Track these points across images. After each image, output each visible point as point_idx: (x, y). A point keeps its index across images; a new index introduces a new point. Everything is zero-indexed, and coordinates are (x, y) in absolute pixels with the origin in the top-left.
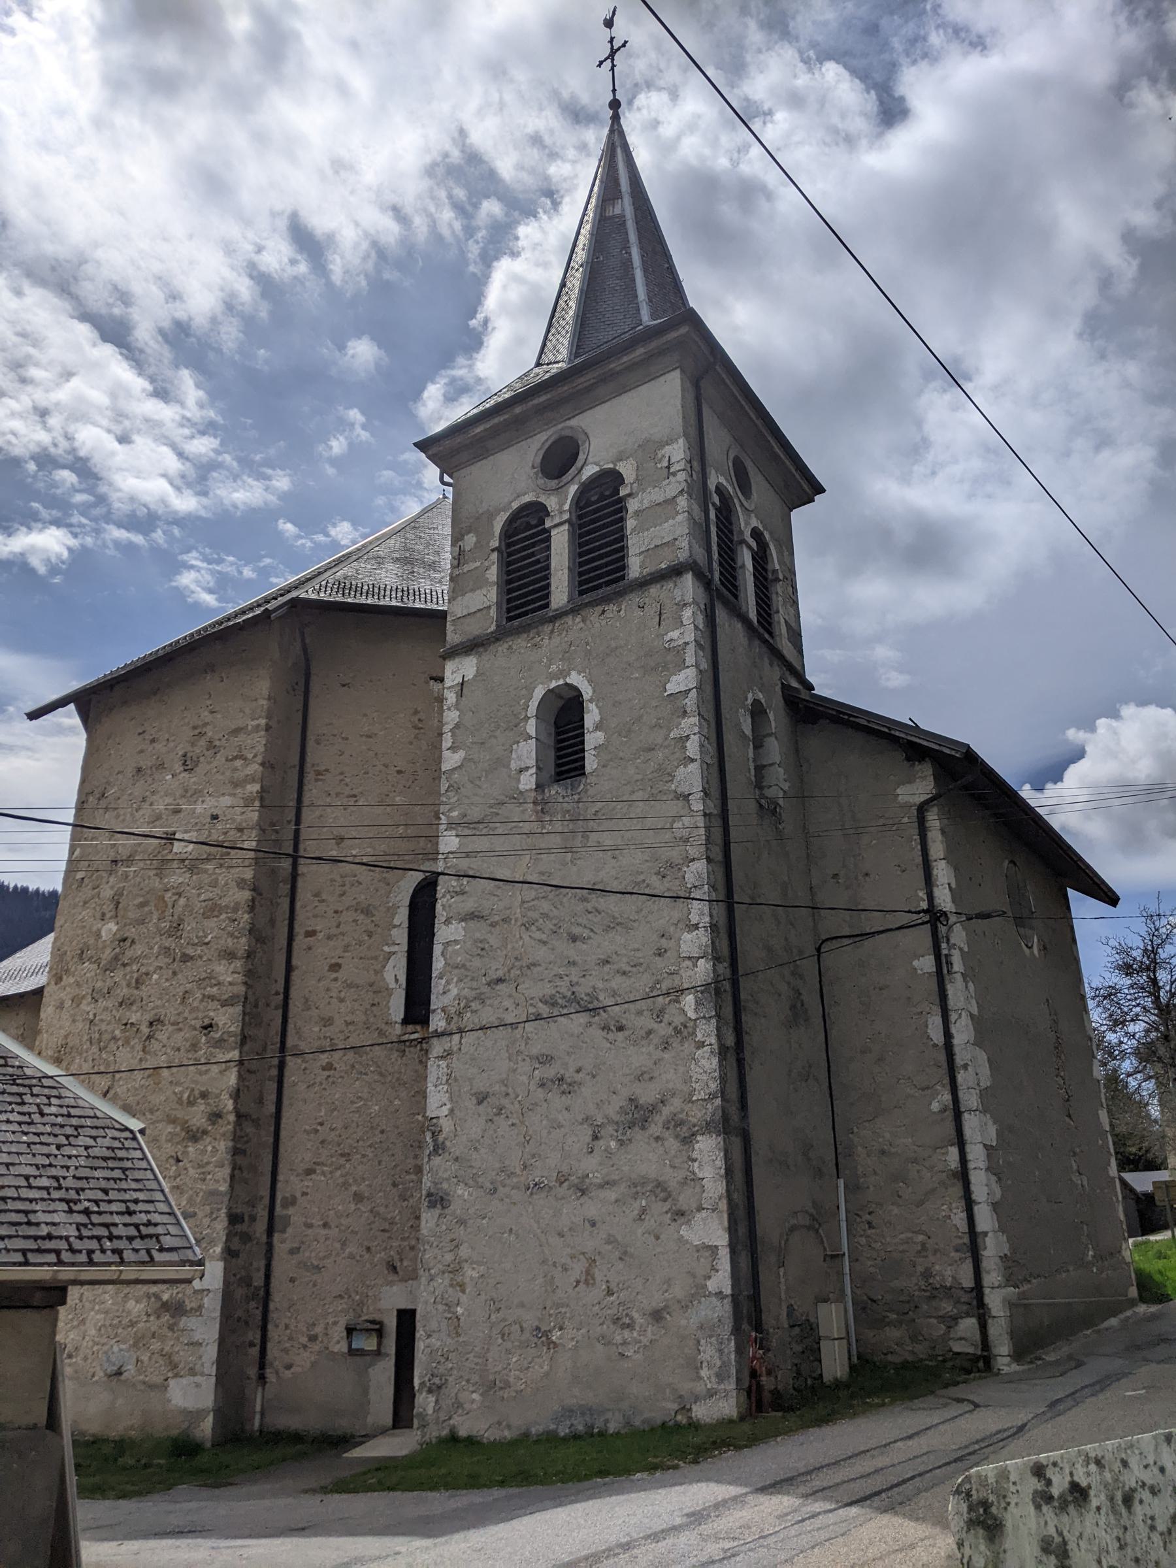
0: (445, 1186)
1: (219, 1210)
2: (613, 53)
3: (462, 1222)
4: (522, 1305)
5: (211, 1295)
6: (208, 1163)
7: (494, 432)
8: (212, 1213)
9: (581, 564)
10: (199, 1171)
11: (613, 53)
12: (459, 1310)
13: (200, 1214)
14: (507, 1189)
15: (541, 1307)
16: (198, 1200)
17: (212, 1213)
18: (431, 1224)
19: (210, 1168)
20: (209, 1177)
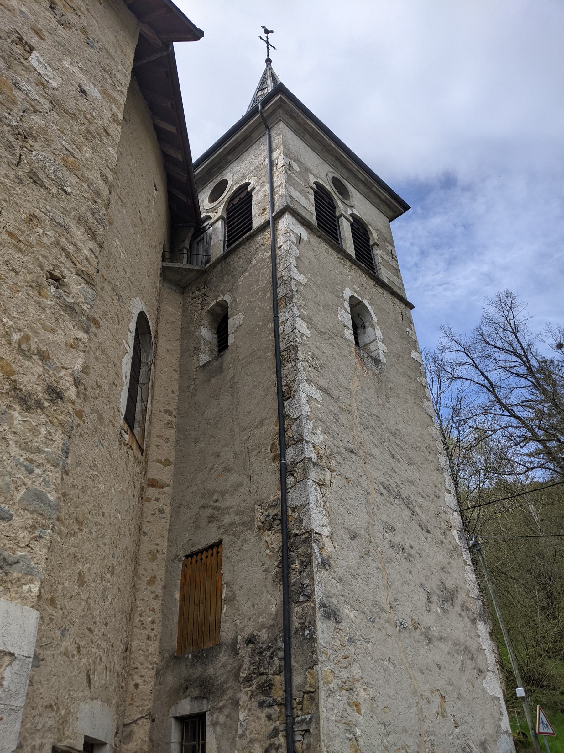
0: (335, 601)
1: (44, 527)
2: (268, 44)
3: (351, 641)
4: (405, 731)
5: (16, 665)
6: (39, 451)
7: (321, 141)
8: (34, 527)
9: (228, 223)
10: (26, 455)
11: (268, 44)
12: (358, 732)
13: (17, 521)
14: (382, 621)
15: (418, 734)
16: (18, 496)
17: (34, 527)
18: (328, 635)
19: (39, 458)
20: (38, 471)
